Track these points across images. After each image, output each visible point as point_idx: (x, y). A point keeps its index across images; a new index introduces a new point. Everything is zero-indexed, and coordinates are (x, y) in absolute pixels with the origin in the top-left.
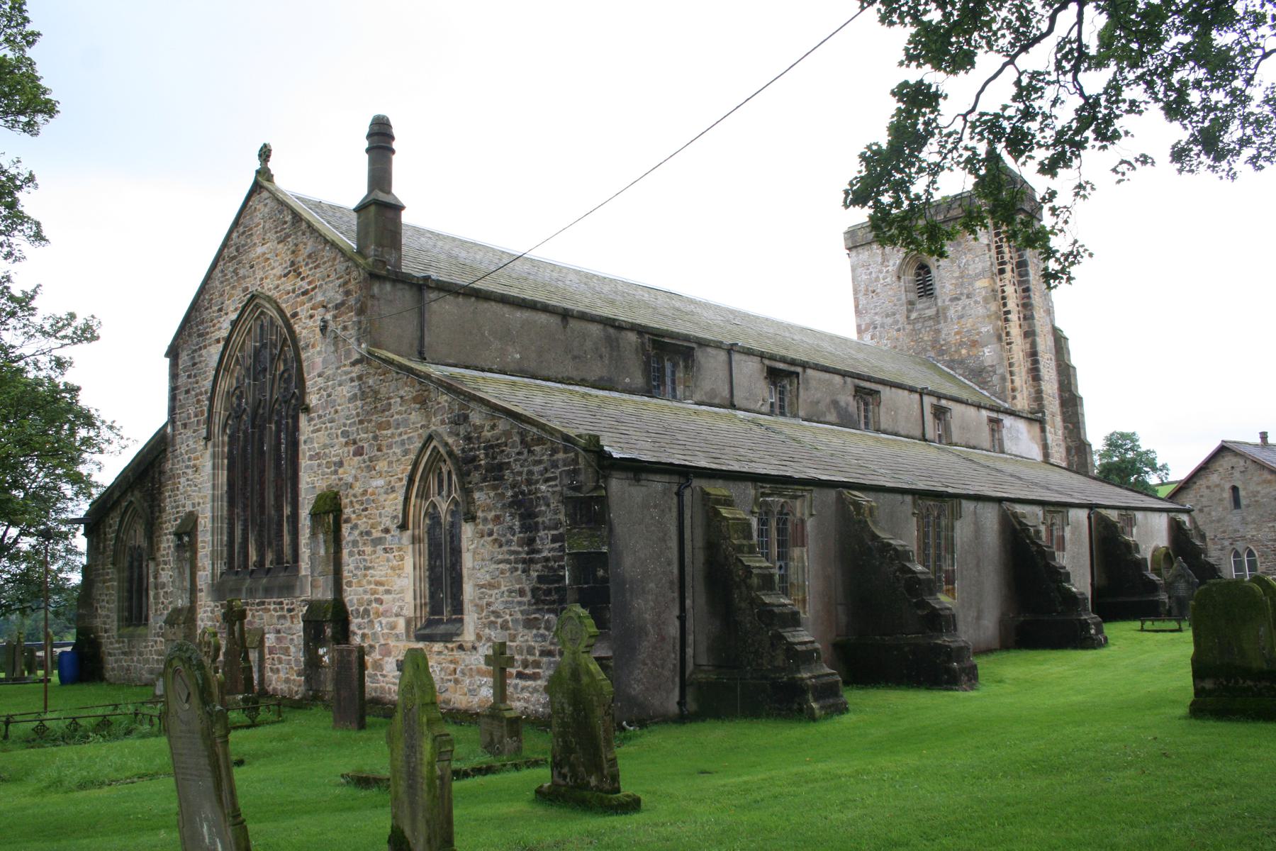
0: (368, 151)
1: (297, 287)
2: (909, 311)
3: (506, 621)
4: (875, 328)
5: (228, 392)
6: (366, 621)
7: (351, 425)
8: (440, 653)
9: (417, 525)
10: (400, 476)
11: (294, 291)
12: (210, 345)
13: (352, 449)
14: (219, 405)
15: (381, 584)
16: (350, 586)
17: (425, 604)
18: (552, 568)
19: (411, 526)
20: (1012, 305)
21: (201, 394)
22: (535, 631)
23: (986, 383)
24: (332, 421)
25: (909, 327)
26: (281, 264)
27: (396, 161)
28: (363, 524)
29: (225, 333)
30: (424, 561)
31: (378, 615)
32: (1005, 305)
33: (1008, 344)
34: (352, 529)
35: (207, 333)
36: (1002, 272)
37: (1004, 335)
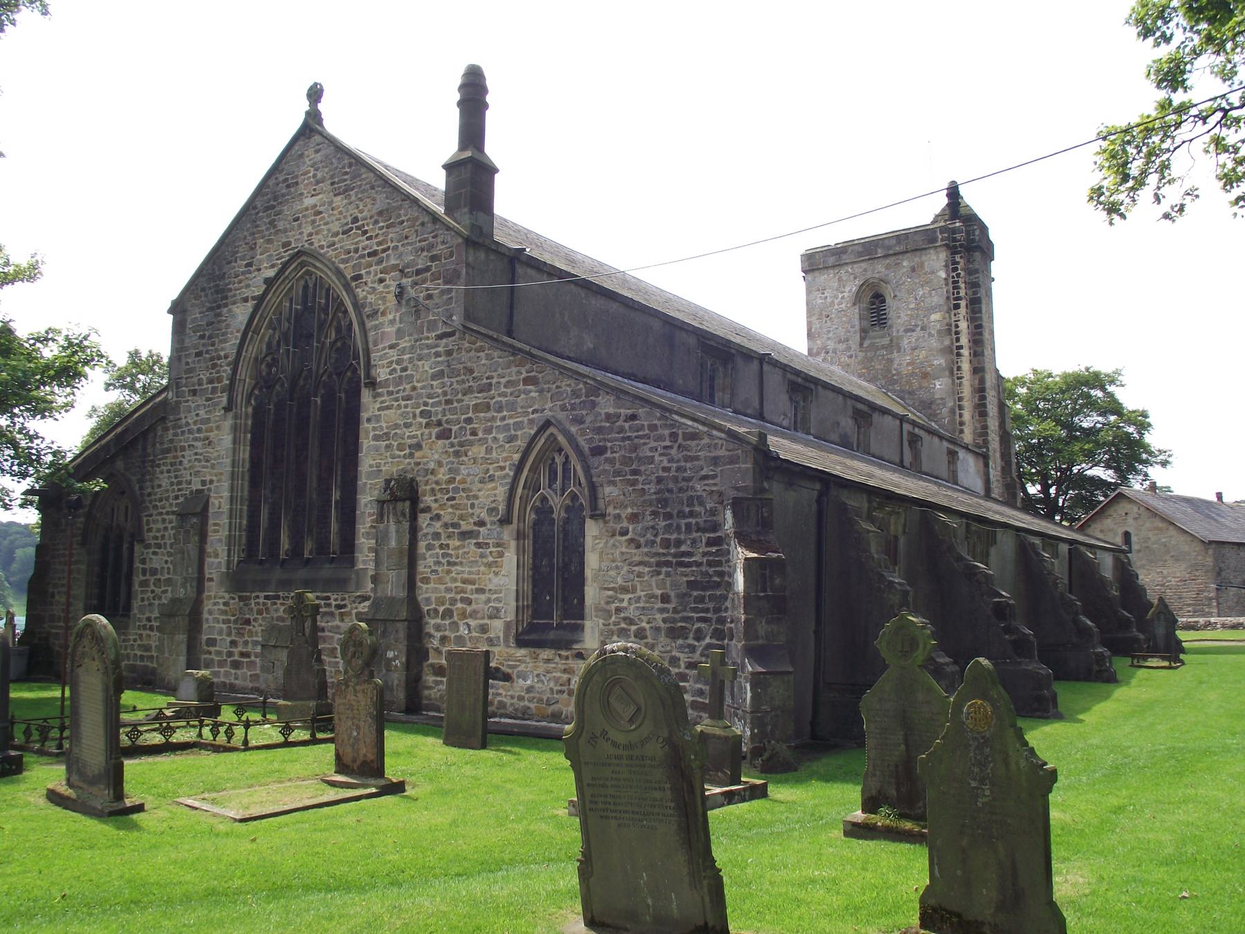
0: (460, 104)
1: (361, 246)
2: (862, 339)
3: (644, 629)
4: (827, 353)
5: (256, 359)
6: (447, 622)
7: (433, 405)
8: (548, 661)
9: (522, 518)
10: (502, 464)
11: (356, 250)
12: (234, 303)
13: (435, 431)
14: (244, 373)
15: (472, 582)
16: (427, 583)
17: (528, 606)
18: (707, 573)
19: (515, 520)
20: (964, 341)
21: (219, 358)
22: (680, 642)
23: (936, 415)
24: (408, 398)
25: (861, 355)
26: (339, 219)
27: (490, 117)
28: (447, 515)
29: (258, 292)
30: (528, 559)
31: (464, 615)
32: (958, 340)
33: (958, 378)
34: (431, 519)
35: (230, 290)
36: (957, 307)
37: (955, 369)
